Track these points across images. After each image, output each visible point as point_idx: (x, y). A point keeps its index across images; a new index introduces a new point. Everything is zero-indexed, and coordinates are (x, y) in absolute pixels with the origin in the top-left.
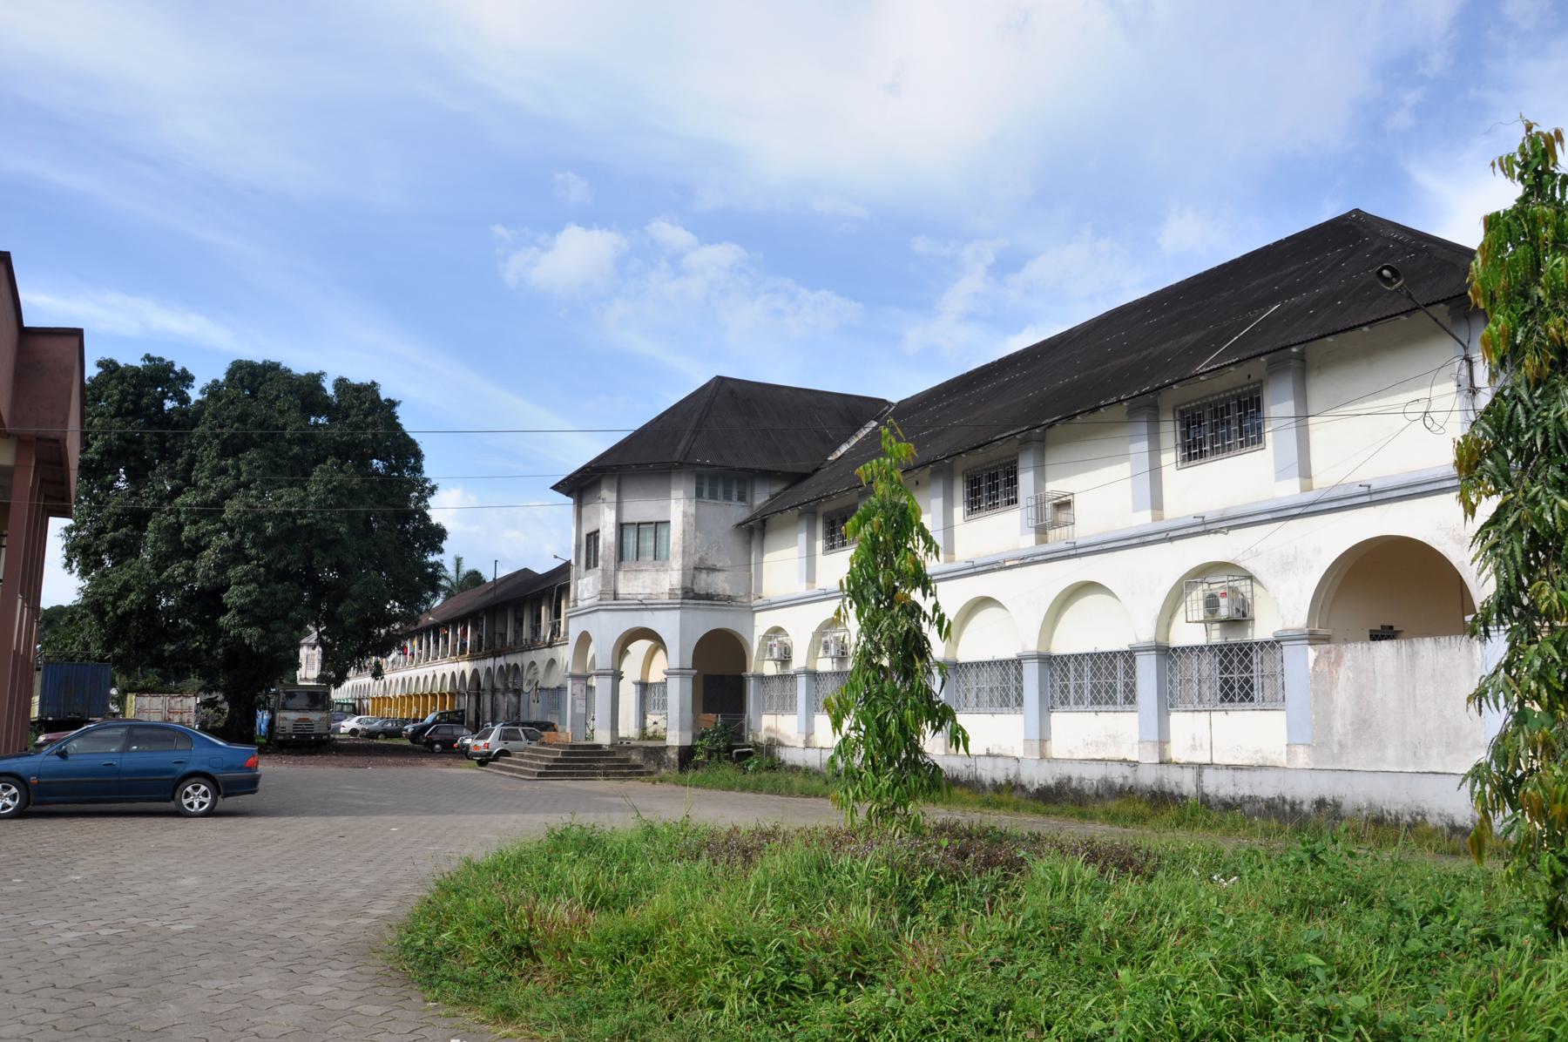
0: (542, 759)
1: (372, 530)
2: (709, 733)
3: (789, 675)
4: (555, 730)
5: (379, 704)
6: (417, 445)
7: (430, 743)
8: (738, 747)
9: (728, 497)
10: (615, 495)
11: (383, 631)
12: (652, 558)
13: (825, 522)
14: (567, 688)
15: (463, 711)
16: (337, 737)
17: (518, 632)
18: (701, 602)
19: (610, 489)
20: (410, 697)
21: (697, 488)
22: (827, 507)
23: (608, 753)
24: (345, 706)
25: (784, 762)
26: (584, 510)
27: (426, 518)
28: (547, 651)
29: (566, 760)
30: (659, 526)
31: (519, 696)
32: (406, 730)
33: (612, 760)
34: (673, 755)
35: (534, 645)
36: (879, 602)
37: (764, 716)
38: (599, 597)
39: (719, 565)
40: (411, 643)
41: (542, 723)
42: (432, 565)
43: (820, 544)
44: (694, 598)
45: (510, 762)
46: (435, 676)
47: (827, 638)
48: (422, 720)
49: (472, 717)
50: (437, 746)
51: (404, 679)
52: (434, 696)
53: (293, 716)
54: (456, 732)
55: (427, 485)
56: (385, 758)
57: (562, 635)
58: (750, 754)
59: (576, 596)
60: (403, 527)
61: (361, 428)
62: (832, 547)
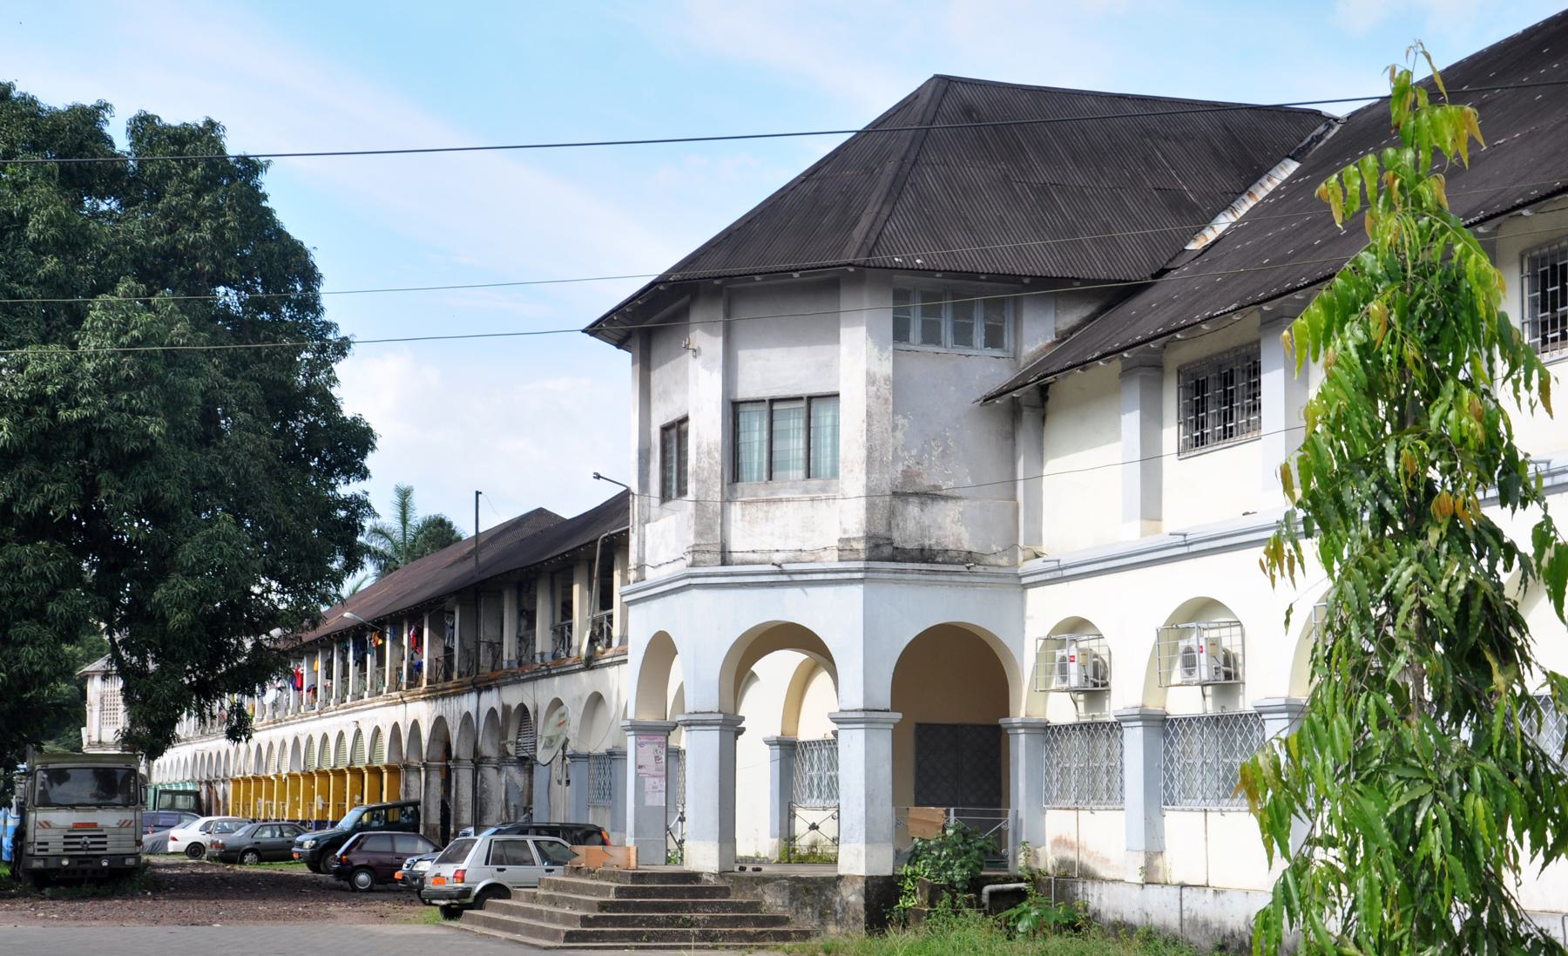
0: (574, 904)
1: (220, 433)
2: (929, 850)
3: (1104, 724)
4: (604, 843)
5: (247, 792)
6: (306, 254)
7: (347, 872)
8: (994, 880)
9: (963, 337)
10: (720, 340)
11: (248, 644)
12: (801, 473)
13: (1184, 388)
14: (625, 754)
15: (416, 804)
16: (161, 860)
17: (526, 640)
18: (909, 566)
19: (708, 327)
20: (309, 776)
21: (896, 322)
22: (1187, 352)
23: (713, 891)
24: (180, 798)
25: (1096, 914)
26: (656, 376)
27: (329, 404)
28: (583, 675)
29: (625, 907)
30: (814, 404)
31: (531, 772)
32: (301, 845)
33: (724, 907)
34: (853, 897)
35: (557, 666)
36: (1383, 518)
37: (1050, 813)
38: (689, 559)
39: (947, 486)
40: (311, 664)
41: (578, 827)
42: (345, 503)
43: (1171, 435)
44: (892, 559)
45: (510, 910)
46: (358, 733)
47: (1192, 641)
48: (334, 824)
49: (435, 817)
50: (363, 877)
51: (296, 740)
52: (358, 773)
53: (63, 819)
54: (401, 847)
55: (331, 336)
56: (253, 903)
57: (615, 643)
58: (1020, 895)
59: (641, 558)
60: (285, 425)
61: (189, 219)
62: (1200, 441)
